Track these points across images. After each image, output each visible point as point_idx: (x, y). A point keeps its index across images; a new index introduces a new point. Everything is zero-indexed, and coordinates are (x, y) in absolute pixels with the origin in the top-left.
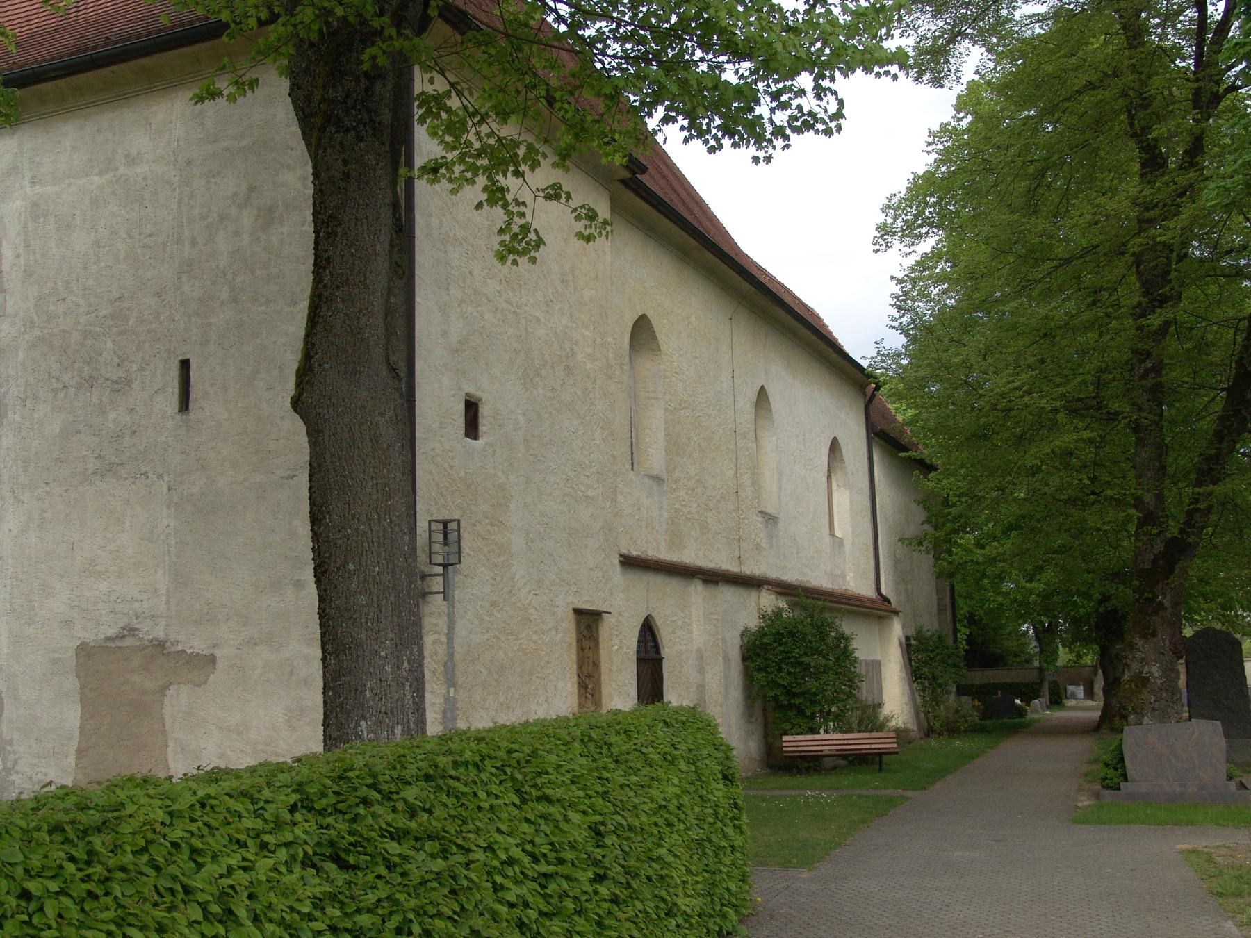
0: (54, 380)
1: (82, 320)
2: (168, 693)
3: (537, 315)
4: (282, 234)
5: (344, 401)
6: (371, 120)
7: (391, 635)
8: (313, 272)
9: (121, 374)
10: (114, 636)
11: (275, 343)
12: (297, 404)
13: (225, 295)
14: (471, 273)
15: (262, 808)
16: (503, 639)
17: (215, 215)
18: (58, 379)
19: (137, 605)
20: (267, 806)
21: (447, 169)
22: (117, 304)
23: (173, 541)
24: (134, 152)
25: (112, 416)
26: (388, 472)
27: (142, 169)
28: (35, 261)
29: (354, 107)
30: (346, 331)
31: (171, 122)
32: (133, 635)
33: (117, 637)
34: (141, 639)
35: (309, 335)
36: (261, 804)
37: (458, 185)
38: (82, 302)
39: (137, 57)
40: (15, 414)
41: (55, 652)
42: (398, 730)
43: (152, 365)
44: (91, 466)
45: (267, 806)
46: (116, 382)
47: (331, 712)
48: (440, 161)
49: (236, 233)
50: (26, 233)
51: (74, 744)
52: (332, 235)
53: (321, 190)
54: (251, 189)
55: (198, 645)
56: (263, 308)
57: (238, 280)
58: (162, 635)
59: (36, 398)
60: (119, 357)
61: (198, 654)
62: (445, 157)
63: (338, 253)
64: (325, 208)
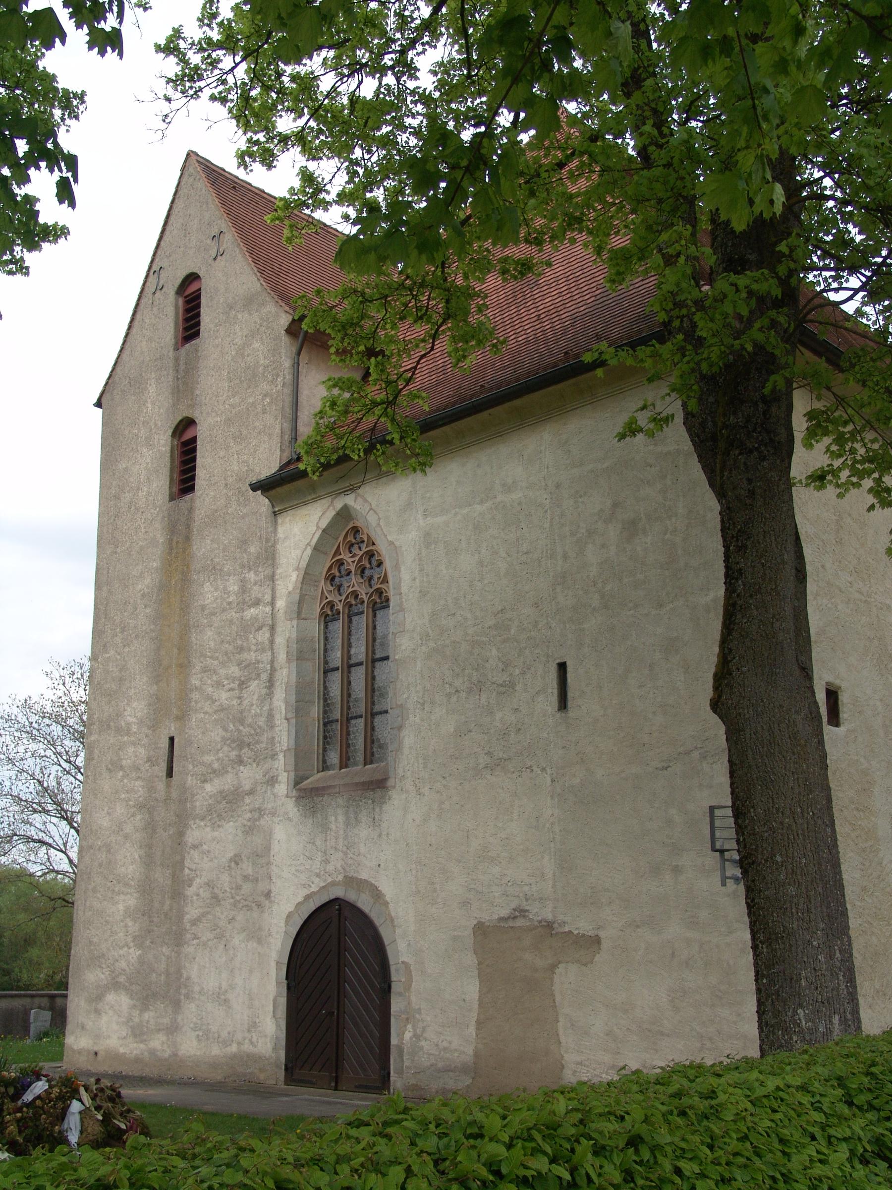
0: (447, 686)
1: (470, 631)
2: (557, 971)
3: (888, 602)
4: (646, 543)
5: (762, 701)
6: (771, 440)
7: (822, 925)
8: (725, 583)
9: (505, 677)
10: (506, 916)
11: (644, 643)
12: (716, 705)
13: (596, 601)
14: (823, 566)
15: (819, 1102)
16: (875, 924)
17: (584, 531)
18: (451, 685)
19: (526, 888)
20: (823, 1100)
21: (833, 475)
22: (500, 615)
23: (557, 829)
24: (510, 481)
25: (499, 715)
26: (808, 767)
27: (517, 495)
28: (429, 582)
29: (754, 430)
30: (761, 635)
31: (541, 452)
32: (524, 916)
33: (509, 918)
34: (531, 920)
35: (724, 642)
36: (818, 1098)
37: (844, 489)
38: (469, 616)
39: (510, 400)
40: (415, 716)
41: (455, 930)
42: (836, 1020)
43: (533, 668)
44: (481, 761)
45: (823, 1100)
46: (502, 685)
47: (767, 999)
48: (826, 469)
49: (603, 546)
50: (420, 559)
51: (474, 1017)
52: (742, 548)
53: (729, 508)
54: (615, 505)
55: (583, 926)
56: (632, 612)
57: (608, 587)
58: (550, 917)
59: (433, 703)
60: (503, 663)
61: (583, 935)
62: (831, 465)
63: (749, 564)
64: (734, 523)
